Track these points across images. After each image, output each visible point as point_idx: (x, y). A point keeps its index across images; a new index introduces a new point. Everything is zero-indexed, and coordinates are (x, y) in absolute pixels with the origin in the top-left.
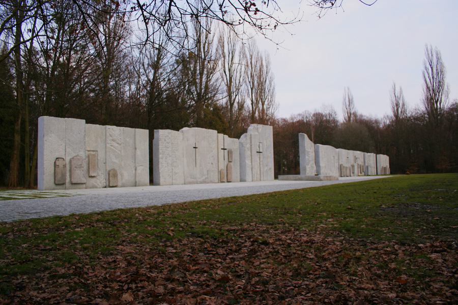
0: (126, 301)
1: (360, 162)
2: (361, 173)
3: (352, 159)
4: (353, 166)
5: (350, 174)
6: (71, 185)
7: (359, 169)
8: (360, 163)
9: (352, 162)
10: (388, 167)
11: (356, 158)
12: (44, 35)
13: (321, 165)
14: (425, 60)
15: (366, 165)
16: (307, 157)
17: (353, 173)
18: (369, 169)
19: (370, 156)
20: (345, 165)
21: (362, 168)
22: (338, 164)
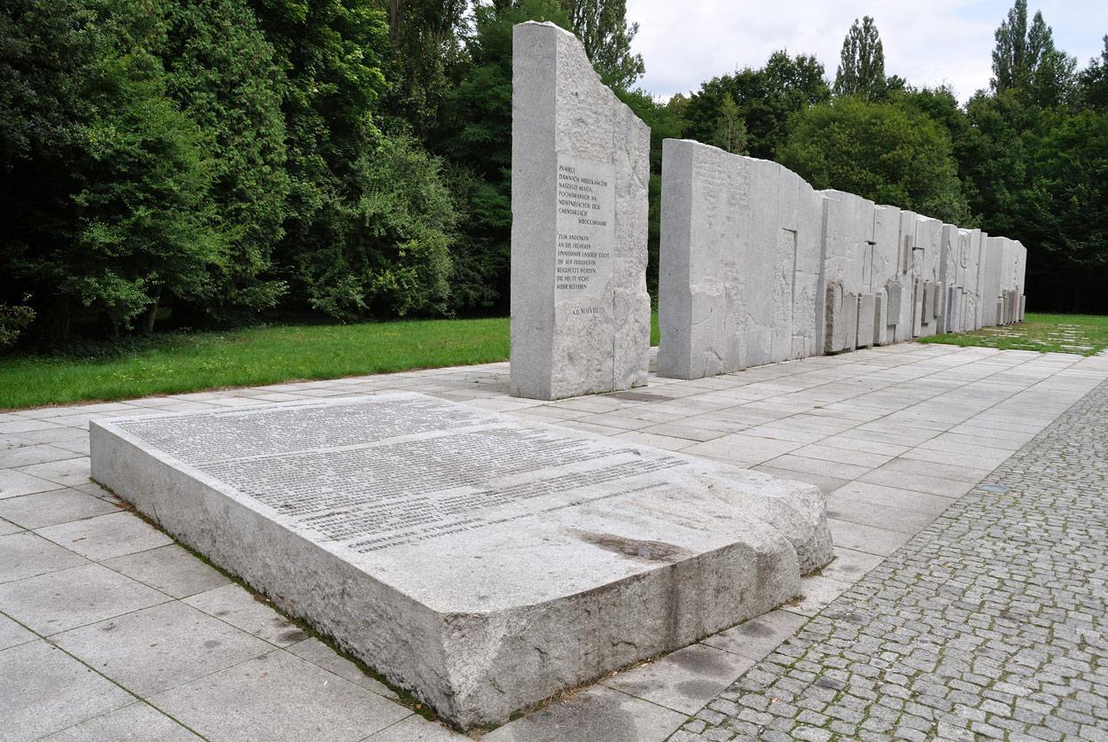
0: (12, 367)
1: (925, 269)
2: (924, 324)
3: (889, 247)
4: (893, 290)
5: (877, 335)
6: (90, 481)
7: (919, 305)
8: (927, 275)
9: (891, 269)
10: (1022, 291)
11: (910, 249)
12: (1105, 719)
13: (695, 288)
14: (840, 67)
15: (949, 281)
16: (565, 224)
17: (892, 327)
18: (960, 300)
19: (965, 241)
20: (854, 286)
21: (930, 298)
22: (814, 278)
